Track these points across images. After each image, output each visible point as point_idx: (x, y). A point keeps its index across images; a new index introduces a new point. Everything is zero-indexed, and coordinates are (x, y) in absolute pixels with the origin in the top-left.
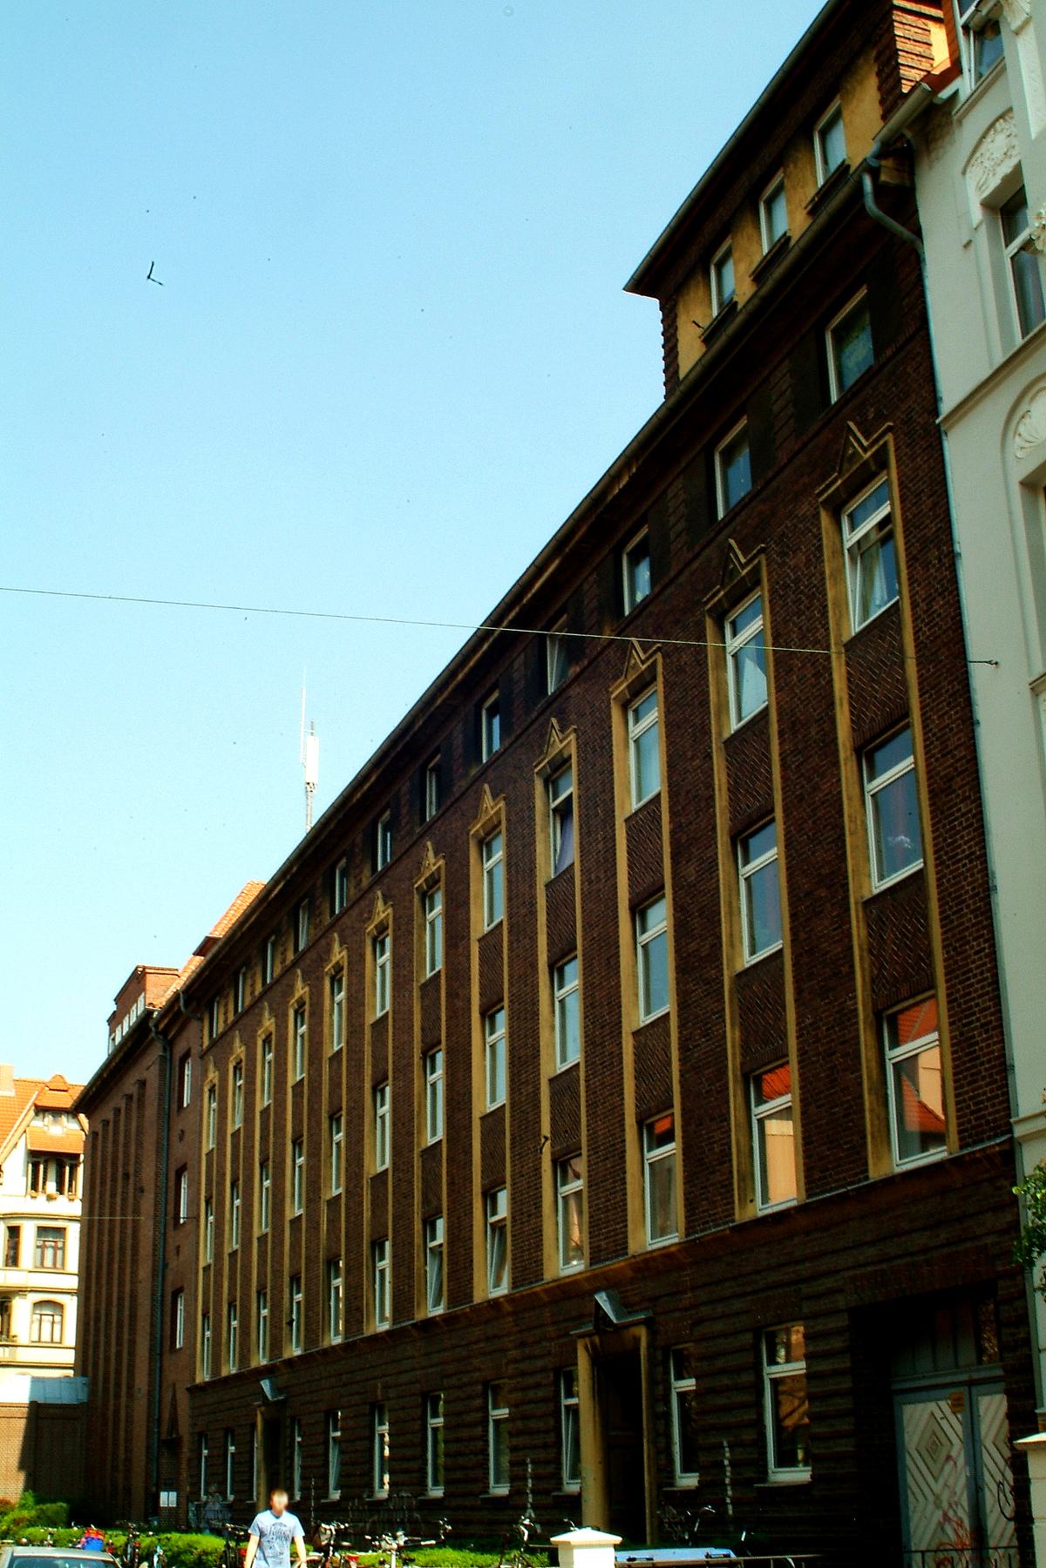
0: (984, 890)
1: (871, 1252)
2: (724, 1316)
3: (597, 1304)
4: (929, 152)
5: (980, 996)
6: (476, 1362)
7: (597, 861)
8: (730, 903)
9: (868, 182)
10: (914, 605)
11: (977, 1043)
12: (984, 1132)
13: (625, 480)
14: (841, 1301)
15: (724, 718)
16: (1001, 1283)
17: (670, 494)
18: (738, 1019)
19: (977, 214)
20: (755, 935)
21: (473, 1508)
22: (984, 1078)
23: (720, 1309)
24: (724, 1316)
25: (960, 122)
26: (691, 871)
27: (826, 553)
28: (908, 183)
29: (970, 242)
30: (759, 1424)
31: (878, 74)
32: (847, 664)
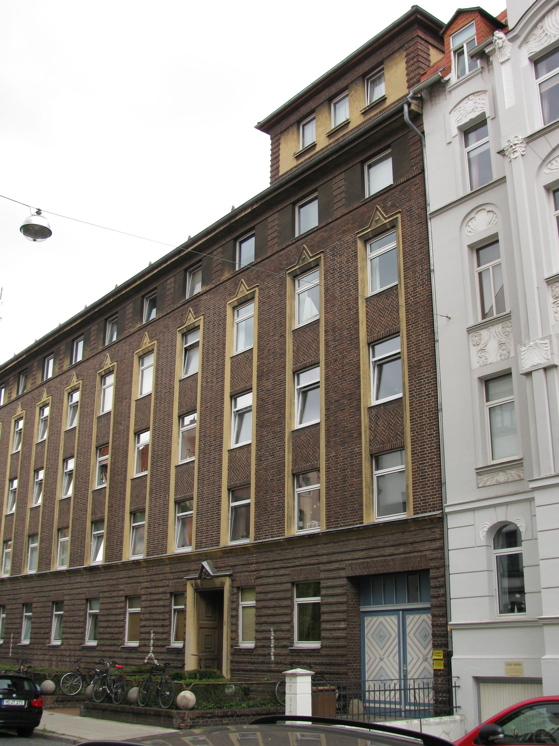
0: (435, 411)
1: (361, 554)
2: (274, 576)
3: (203, 567)
4: (431, 101)
5: (429, 453)
6: (122, 587)
7: (212, 374)
8: (291, 400)
9: (406, 108)
10: (406, 288)
11: (426, 472)
12: (427, 509)
13: (249, 210)
14: (343, 573)
15: (293, 321)
16: (431, 571)
17: (270, 220)
18: (291, 451)
19: (455, 131)
20: (305, 415)
21: (115, 651)
22: (429, 487)
23: (272, 573)
24: (274, 576)
25: (450, 92)
26: (268, 384)
27: (359, 259)
28: (420, 112)
29: (450, 142)
30: (291, 622)
31: (406, 63)
32: (367, 307)
